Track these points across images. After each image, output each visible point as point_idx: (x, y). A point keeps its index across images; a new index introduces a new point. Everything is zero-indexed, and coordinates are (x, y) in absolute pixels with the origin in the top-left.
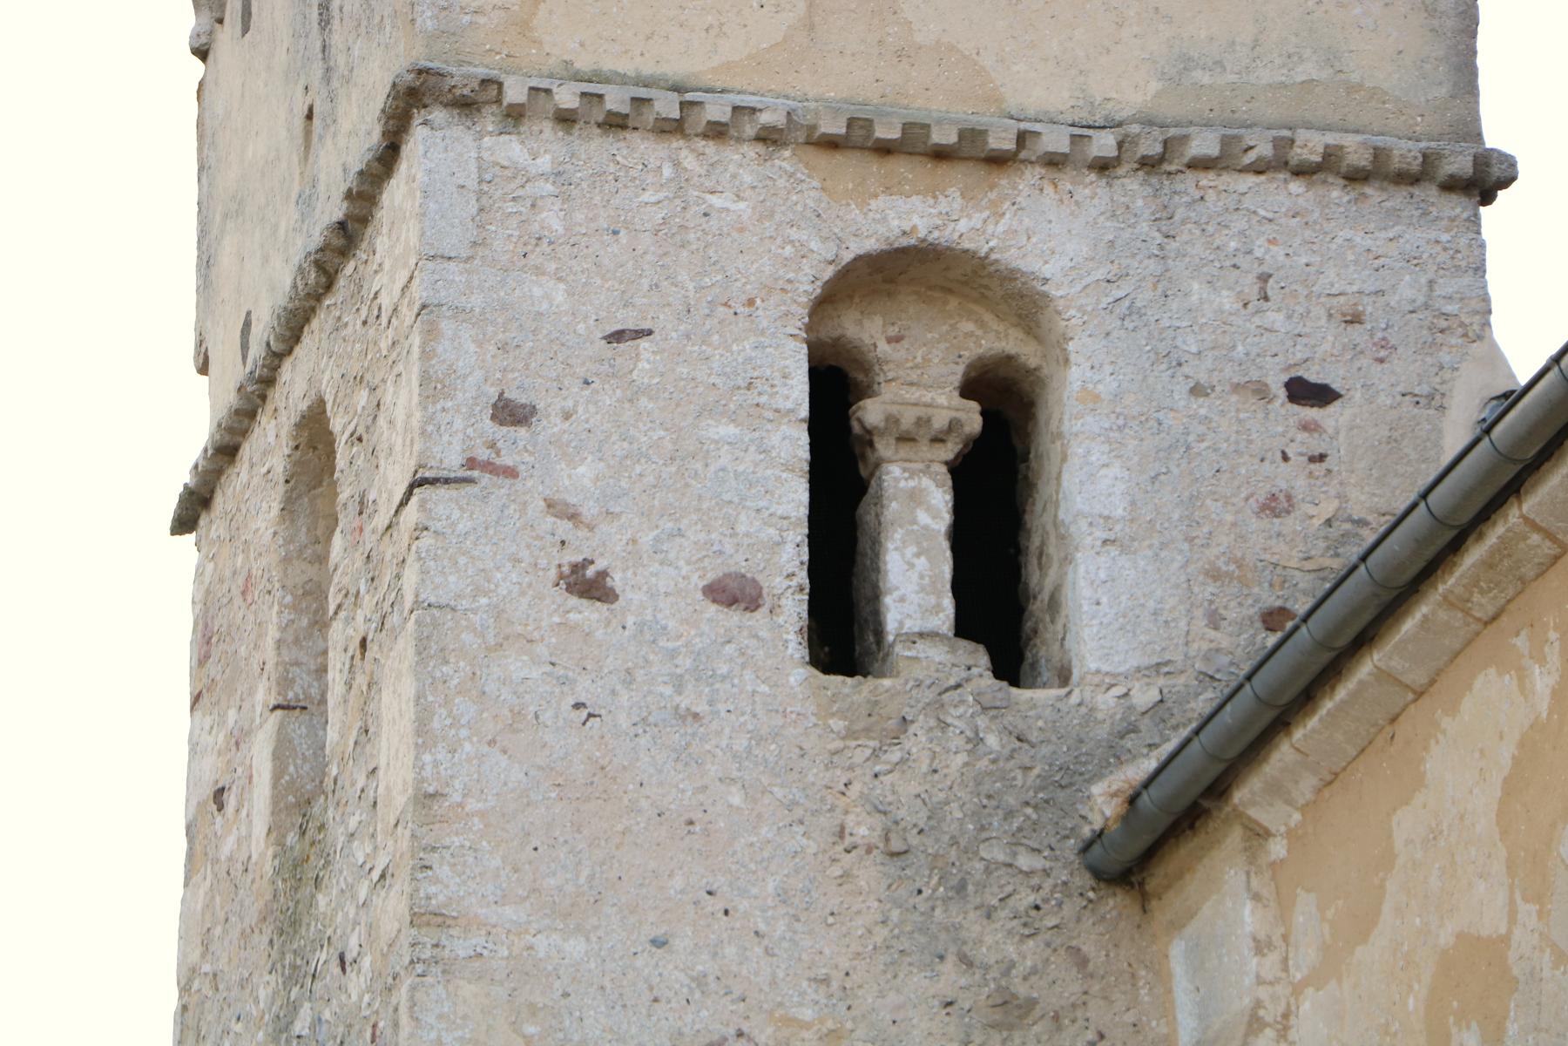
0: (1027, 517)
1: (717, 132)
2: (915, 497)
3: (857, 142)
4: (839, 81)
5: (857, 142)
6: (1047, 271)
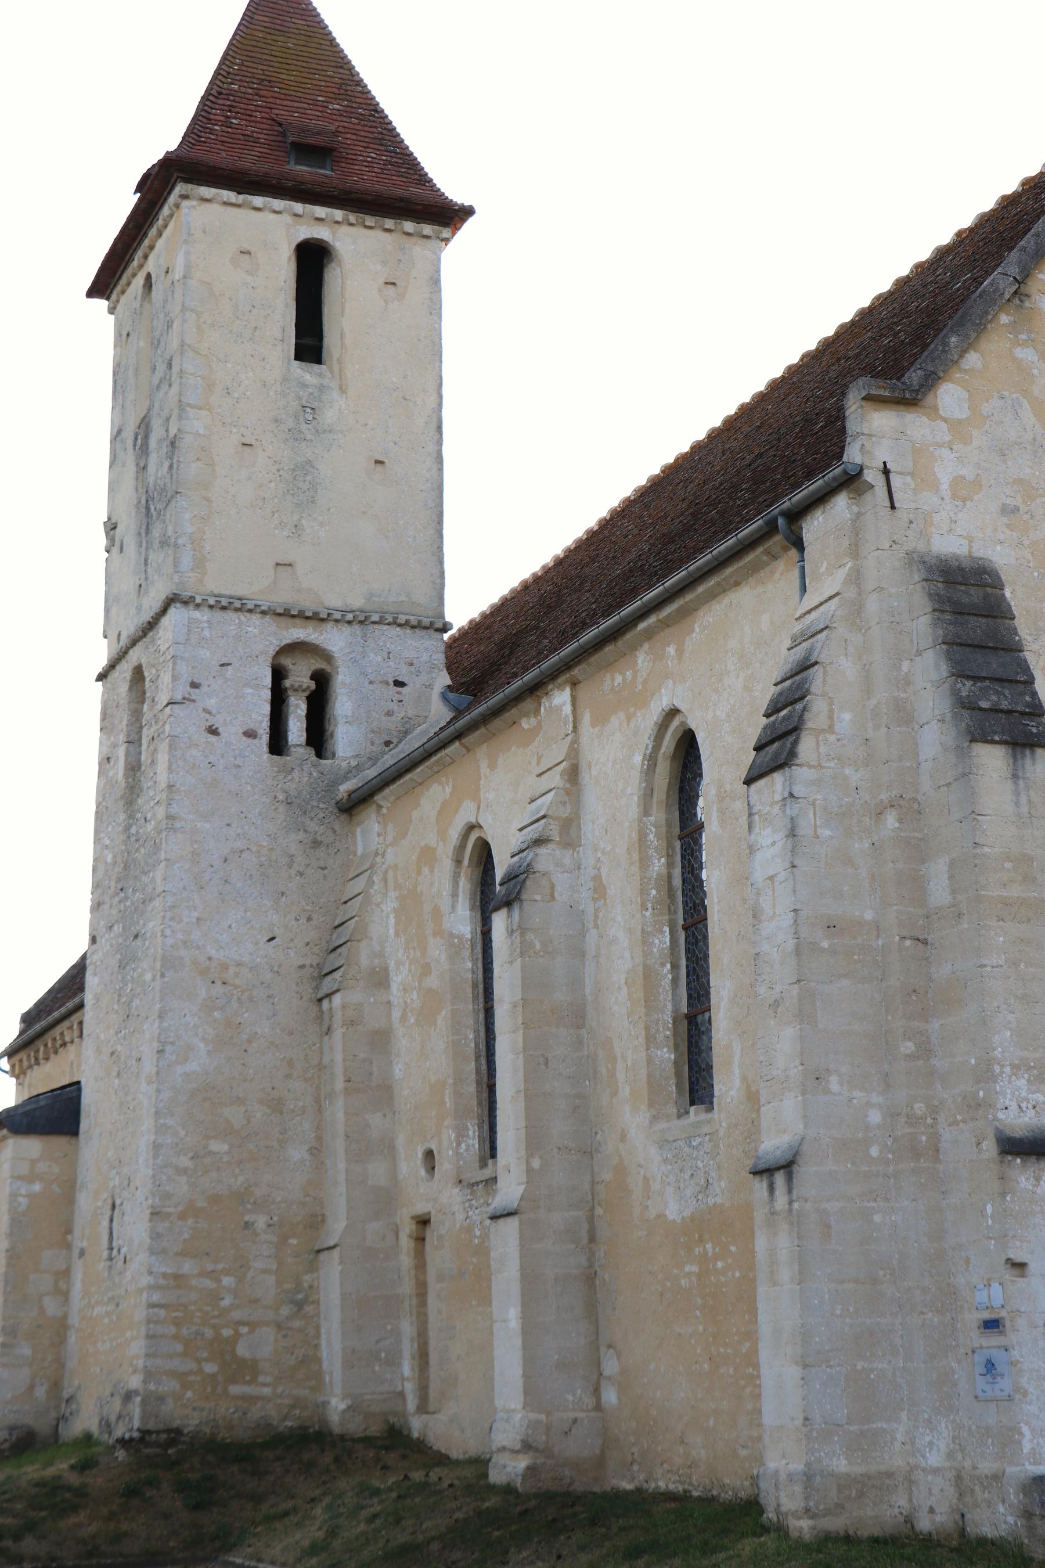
0: (326, 270)
1: (250, 611)
2: (297, 706)
3: (286, 614)
4: (283, 597)
5: (286, 614)
6: (334, 649)
